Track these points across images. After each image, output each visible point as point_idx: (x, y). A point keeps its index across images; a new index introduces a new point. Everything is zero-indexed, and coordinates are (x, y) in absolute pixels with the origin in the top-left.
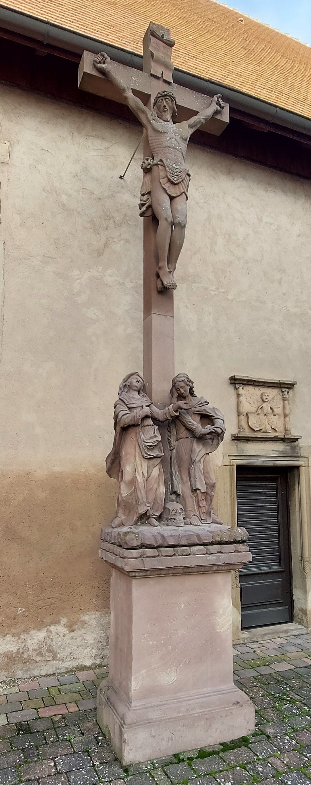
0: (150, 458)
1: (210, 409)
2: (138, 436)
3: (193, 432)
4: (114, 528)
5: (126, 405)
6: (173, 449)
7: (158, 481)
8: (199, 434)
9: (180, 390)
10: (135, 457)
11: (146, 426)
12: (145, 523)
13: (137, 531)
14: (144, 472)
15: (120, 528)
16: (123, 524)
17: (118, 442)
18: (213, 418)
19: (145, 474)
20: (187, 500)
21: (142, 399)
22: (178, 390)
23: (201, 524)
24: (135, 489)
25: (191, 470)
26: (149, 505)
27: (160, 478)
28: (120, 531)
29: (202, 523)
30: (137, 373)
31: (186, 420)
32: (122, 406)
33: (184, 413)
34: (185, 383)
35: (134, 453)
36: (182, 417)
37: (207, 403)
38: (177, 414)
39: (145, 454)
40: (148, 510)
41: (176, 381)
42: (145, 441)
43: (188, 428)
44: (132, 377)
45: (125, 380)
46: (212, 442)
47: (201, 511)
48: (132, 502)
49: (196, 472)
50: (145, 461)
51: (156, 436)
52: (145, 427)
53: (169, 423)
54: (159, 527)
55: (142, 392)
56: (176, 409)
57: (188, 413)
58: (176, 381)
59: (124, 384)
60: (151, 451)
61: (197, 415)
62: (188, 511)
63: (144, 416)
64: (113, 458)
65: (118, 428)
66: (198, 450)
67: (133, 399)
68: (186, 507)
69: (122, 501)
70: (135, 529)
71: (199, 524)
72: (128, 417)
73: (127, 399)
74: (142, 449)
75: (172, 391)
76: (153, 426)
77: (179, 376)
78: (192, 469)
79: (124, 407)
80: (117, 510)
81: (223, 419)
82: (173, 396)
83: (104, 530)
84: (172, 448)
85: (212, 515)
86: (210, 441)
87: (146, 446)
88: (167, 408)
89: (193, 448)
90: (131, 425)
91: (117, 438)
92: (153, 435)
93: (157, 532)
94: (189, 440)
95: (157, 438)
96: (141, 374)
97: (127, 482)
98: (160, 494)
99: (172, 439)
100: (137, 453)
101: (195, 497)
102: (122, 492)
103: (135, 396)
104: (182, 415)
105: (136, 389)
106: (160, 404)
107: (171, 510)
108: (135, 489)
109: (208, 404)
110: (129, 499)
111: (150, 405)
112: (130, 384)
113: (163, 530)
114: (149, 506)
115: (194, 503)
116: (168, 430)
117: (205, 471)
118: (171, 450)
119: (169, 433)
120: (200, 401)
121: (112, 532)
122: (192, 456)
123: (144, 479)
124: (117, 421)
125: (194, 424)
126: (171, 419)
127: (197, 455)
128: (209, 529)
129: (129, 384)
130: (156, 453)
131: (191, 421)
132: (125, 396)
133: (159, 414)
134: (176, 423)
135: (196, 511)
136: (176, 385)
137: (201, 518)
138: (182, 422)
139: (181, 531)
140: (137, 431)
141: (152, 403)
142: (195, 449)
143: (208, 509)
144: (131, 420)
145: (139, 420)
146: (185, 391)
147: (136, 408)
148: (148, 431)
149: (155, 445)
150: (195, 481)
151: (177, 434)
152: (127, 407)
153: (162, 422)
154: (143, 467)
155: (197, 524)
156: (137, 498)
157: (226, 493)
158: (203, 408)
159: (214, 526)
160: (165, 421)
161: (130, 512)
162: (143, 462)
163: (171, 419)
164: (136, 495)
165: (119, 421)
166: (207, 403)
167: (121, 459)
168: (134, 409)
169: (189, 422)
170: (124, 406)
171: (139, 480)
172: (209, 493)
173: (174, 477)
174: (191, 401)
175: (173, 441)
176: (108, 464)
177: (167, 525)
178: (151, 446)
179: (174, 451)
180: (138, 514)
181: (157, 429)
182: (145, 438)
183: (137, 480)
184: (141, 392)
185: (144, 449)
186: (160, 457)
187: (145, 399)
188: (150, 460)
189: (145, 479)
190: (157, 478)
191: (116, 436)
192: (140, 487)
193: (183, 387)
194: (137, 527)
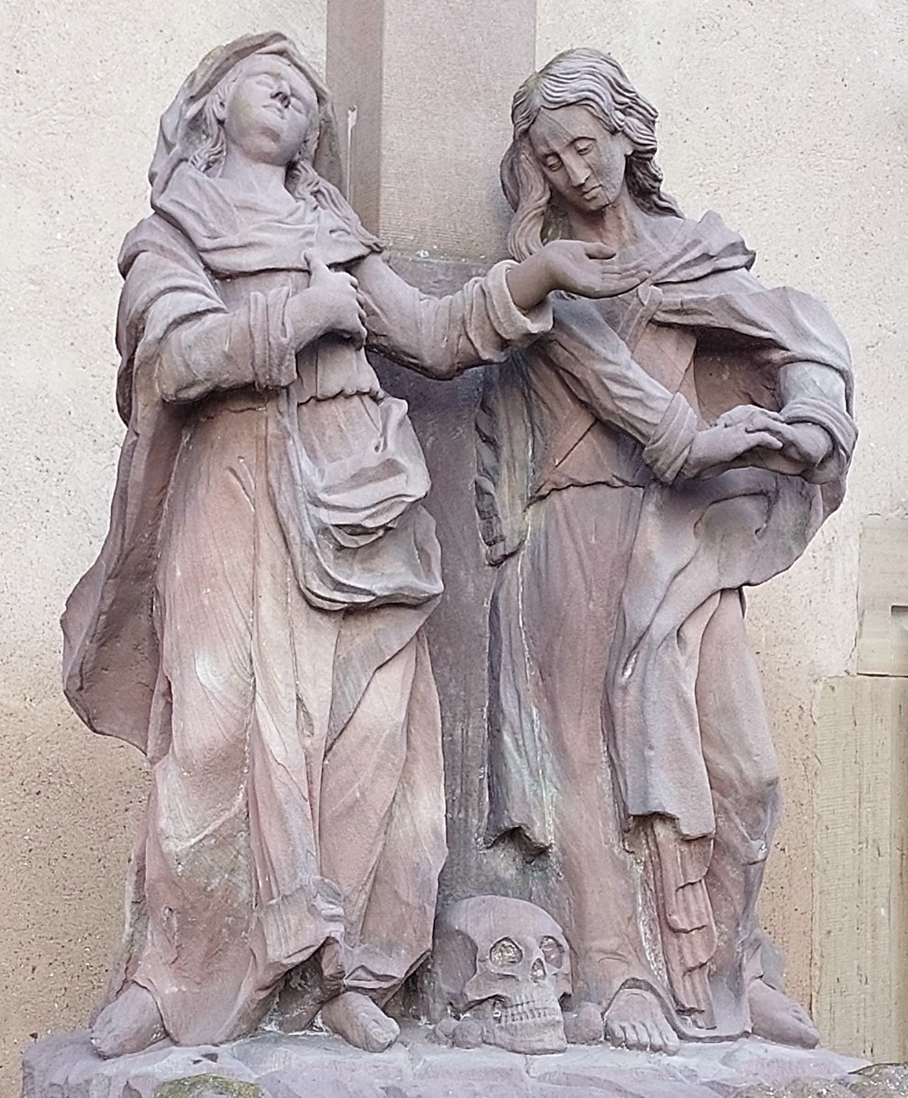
0: (352, 612)
1: (756, 297)
2: (273, 462)
3: (643, 447)
4: (103, 1057)
5: (198, 252)
6: (506, 557)
7: (399, 761)
8: (680, 462)
9: (562, 164)
10: (254, 599)
11: (326, 399)
12: (311, 1025)
13: (252, 1077)
14: (312, 706)
15: (140, 1056)
16: (167, 1034)
17: (144, 500)
18: (776, 356)
19: (318, 708)
20: (590, 885)
21: (310, 216)
22: (551, 161)
23: (673, 1040)
24: (252, 803)
25: (619, 693)
26: (339, 911)
27: (417, 742)
28: (137, 1077)
29: (682, 1036)
30: (279, 37)
31: (598, 366)
32: (174, 265)
33: (586, 320)
34: (600, 119)
35: (248, 571)
36: (571, 344)
37: (741, 260)
38: (535, 326)
39: (316, 585)
40: (328, 942)
41: (538, 101)
42: (323, 497)
43: (605, 417)
44: (245, 65)
45: (200, 82)
46: (769, 513)
47: (675, 959)
48: (231, 890)
49: (649, 708)
50: (318, 628)
51: (391, 468)
52: (325, 405)
53: (487, 384)
54: (398, 1056)
55: (312, 172)
56: (531, 292)
57: (612, 321)
58: (538, 101)
59: (193, 109)
60: (362, 562)
61: (674, 334)
62: (598, 957)
63: (309, 338)
64: (108, 602)
65: (143, 408)
66: (666, 565)
67: (250, 214)
68: (581, 926)
69: (162, 887)
70: (236, 1065)
71: (658, 1041)
72: (208, 332)
73: (209, 215)
74: (296, 550)
75: (512, 170)
76: (375, 399)
77: (555, 70)
78: (625, 689)
79: (181, 270)
80: (131, 941)
81: (842, 365)
82: (515, 206)
83: (44, 1072)
84: (500, 549)
85: (753, 987)
86: (751, 508)
87: (325, 530)
88: (472, 287)
89: (639, 550)
90: (231, 389)
91: (139, 472)
92: (372, 459)
93: (379, 1083)
94: (613, 499)
95: (401, 479)
96: (317, 62)
97: (197, 758)
98: (416, 842)
99: (506, 489)
100: (265, 578)
101: (640, 869)
102: (163, 823)
103: (261, 198)
104: (572, 335)
105: (269, 146)
106: (432, 253)
107: (484, 946)
108: (252, 803)
109: (748, 267)
110: (210, 873)
111: (361, 258)
112: (231, 111)
113: (425, 1074)
114: (332, 919)
115: (635, 901)
116: (477, 428)
117: (711, 702)
118: (496, 564)
119: (486, 451)
120: (696, 242)
121: (88, 1082)
122: (626, 601)
123: (308, 742)
124: (136, 362)
125: (648, 395)
126: (497, 357)
127: (660, 593)
128: (724, 1073)
129: (222, 114)
130: (391, 575)
131: (630, 375)
132: (192, 189)
133: (417, 325)
134: (529, 385)
135: (650, 957)
136: (539, 129)
137: (677, 1002)
138: (566, 376)
139: (539, 1079)
140: (272, 429)
141: (376, 250)
142: (649, 556)
143: (729, 944)
144: (228, 357)
145: (282, 359)
146: (597, 172)
147: (264, 279)
148: (343, 437)
149: (386, 528)
150: (645, 762)
151: (540, 462)
152: (207, 267)
153: (441, 377)
154: (307, 667)
155: (645, 1039)
156: (264, 867)
157: (871, 851)
158: (714, 288)
159: (761, 1052)
160: (460, 371)
161: (213, 954)
162: (305, 637)
163: (497, 357)
164: (254, 845)
165: (149, 361)
166: (741, 260)
167: (163, 609)
168: (253, 281)
169: (616, 379)
170: (187, 266)
171: (276, 748)
172: (736, 841)
173: (507, 738)
174: (636, 237)
175: (512, 505)
176: (78, 642)
177: (455, 1040)
178: (356, 530)
179: (517, 569)
180: (261, 968)
181: (401, 424)
182: (322, 472)
183: (263, 748)
184: (307, 172)
185: (312, 550)
186: (416, 605)
187: (328, 218)
188: (351, 621)
189: (318, 742)
190: (392, 736)
191: (127, 454)
192: (281, 792)
193: (581, 145)
194: (255, 1050)
